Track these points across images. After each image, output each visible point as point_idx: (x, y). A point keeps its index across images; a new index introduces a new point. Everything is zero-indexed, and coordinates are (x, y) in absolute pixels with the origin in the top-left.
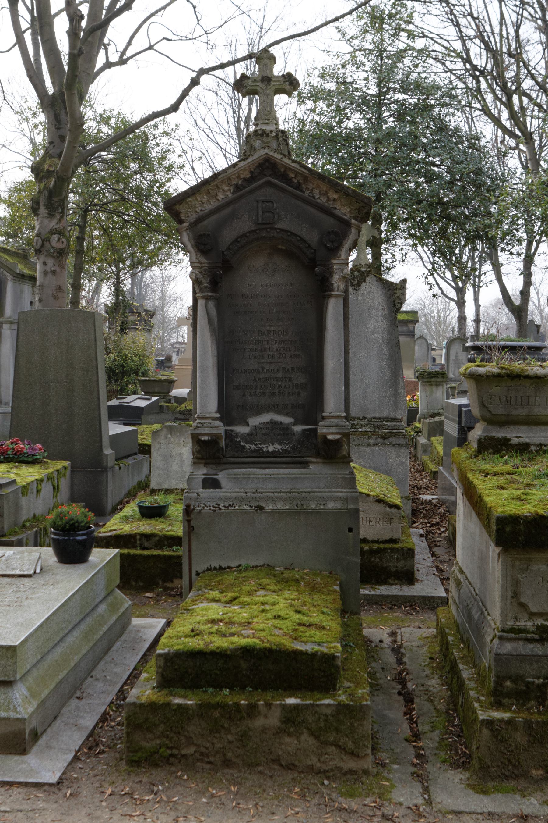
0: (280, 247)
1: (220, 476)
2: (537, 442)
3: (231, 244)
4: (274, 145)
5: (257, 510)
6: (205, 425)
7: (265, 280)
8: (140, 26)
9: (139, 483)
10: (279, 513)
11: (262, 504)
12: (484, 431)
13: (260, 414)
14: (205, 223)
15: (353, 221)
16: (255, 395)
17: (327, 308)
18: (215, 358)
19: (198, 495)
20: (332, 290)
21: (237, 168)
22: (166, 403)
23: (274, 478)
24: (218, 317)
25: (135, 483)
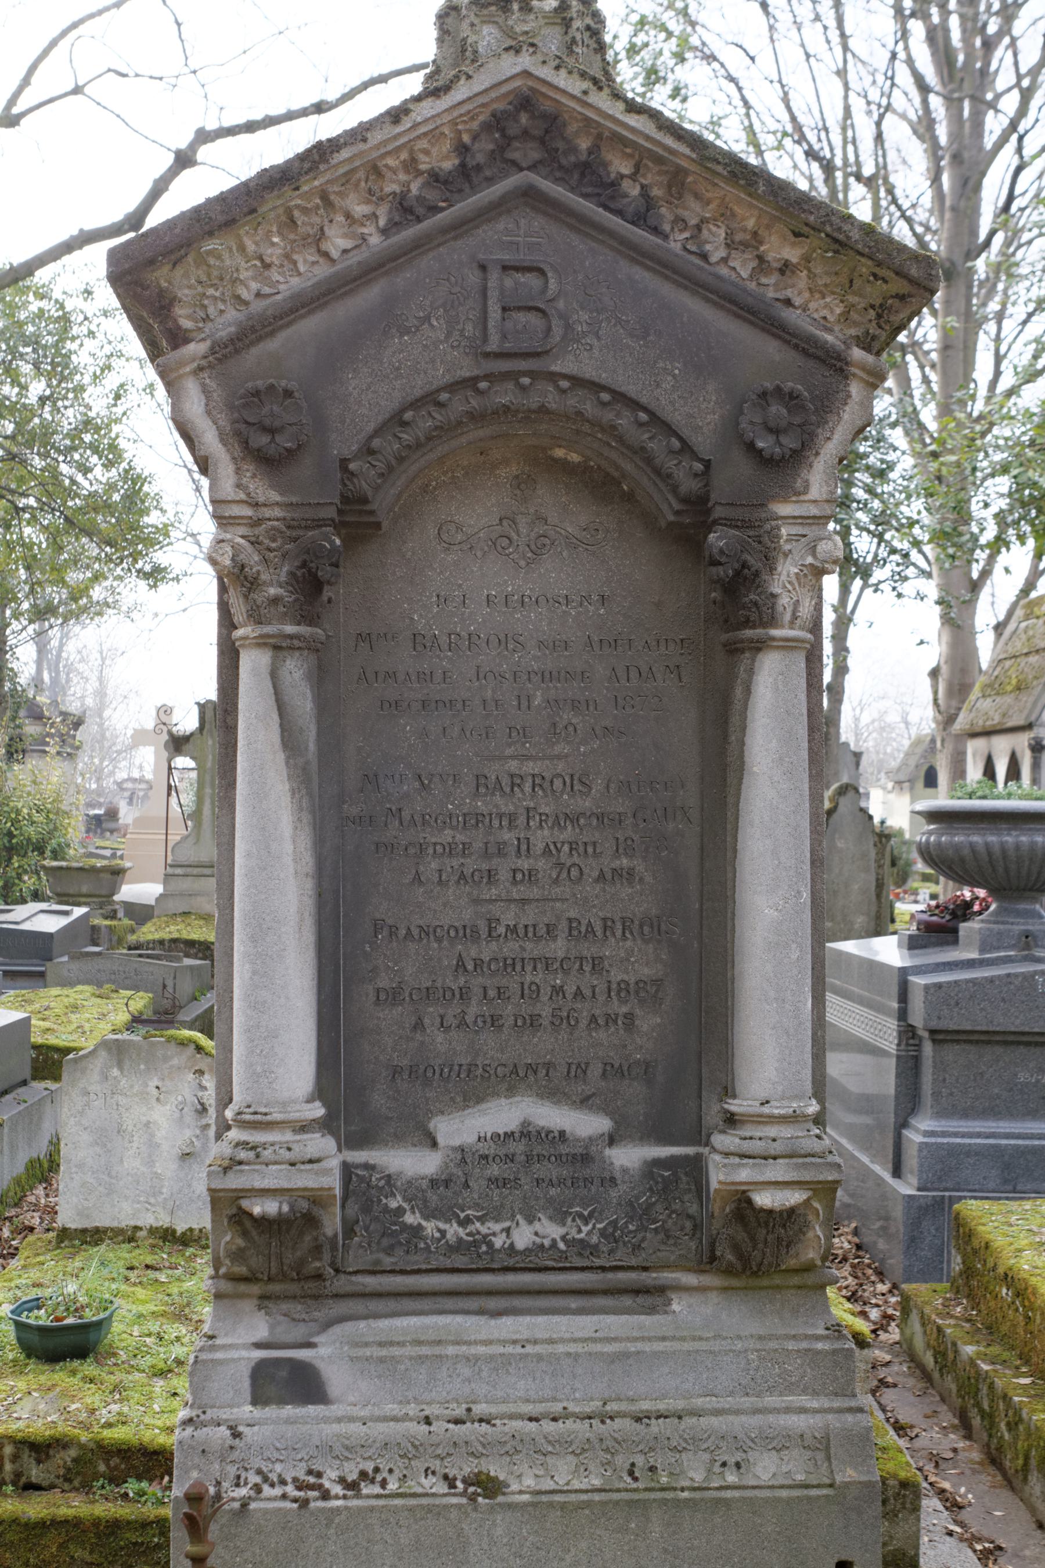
0: (559, 453)
1: (323, 1351)
3: (377, 432)
4: (552, 42)
5: (473, 1498)
6: (267, 1154)
7: (504, 583)
8: (53, 43)
9: (33, 1164)
10: (563, 1506)
11: (495, 1469)
13: (480, 1100)
14: (273, 345)
15: (857, 354)
16: (462, 1024)
17: (748, 691)
18: (309, 884)
19: (236, 1435)
20: (773, 621)
21: (406, 123)
22: (106, 918)
23: (539, 1358)
24: (319, 723)
25: (20, 1168)
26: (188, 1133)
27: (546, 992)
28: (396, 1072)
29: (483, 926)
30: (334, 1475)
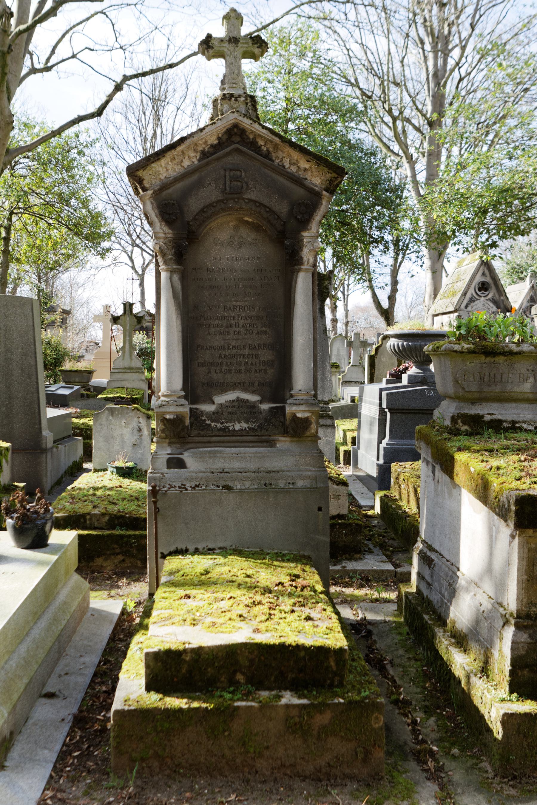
2: (510, 418)
3: (197, 214)
8: (63, 36)
10: (248, 493)
12: (457, 408)
13: (226, 392)
14: (170, 191)
15: (324, 193)
16: (221, 372)
17: (296, 283)
18: (180, 334)
21: (204, 131)
26: (135, 438)
27: (243, 363)
28: (203, 384)
29: (226, 346)
30: (189, 485)
